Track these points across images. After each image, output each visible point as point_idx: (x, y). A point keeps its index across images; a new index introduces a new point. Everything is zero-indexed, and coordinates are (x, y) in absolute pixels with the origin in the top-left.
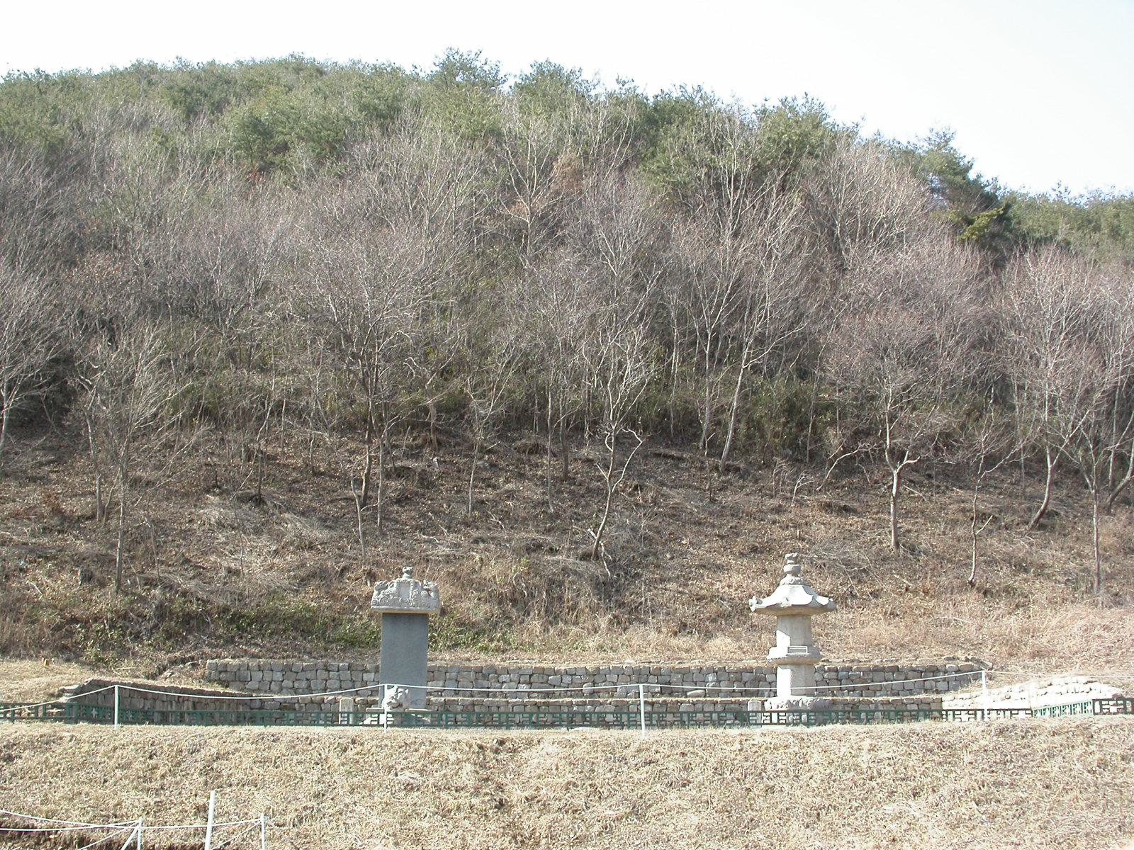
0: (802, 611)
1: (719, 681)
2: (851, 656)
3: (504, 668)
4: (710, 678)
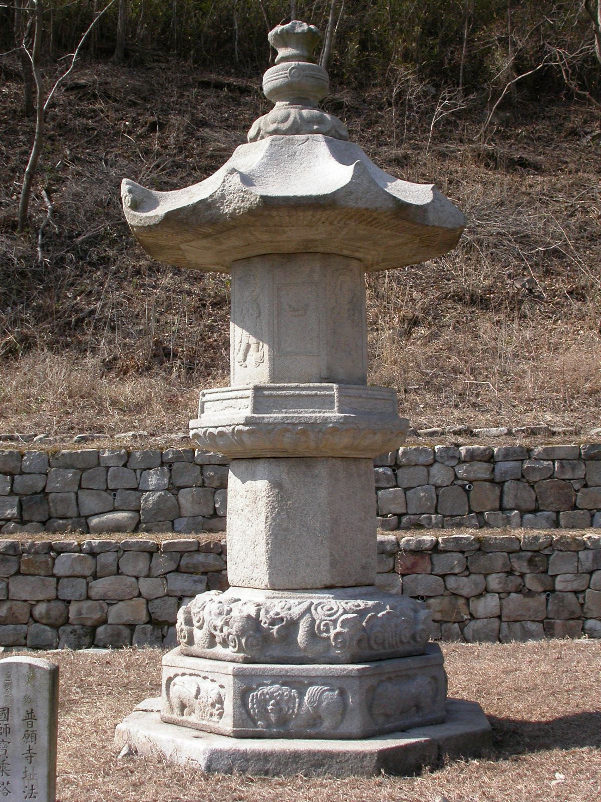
0: (319, 232)
1: (174, 489)
2: (528, 420)
4: (153, 479)
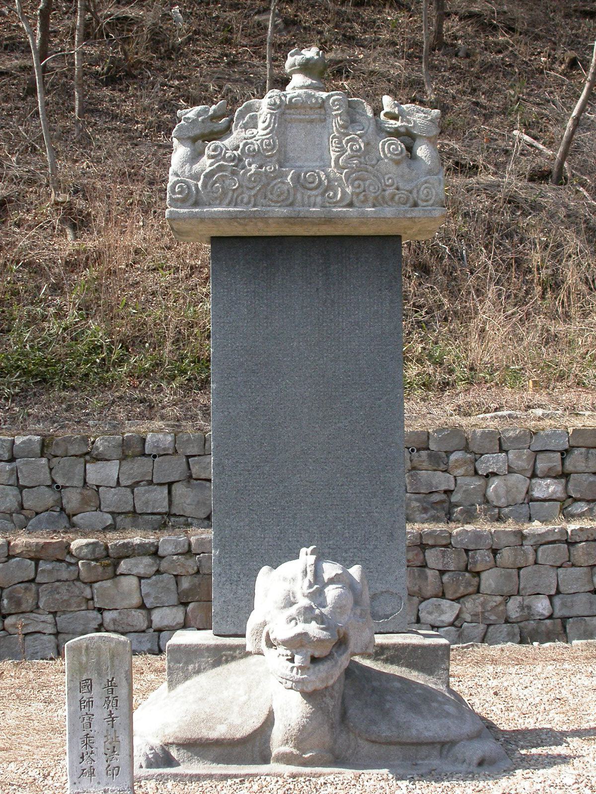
3: (488, 435)
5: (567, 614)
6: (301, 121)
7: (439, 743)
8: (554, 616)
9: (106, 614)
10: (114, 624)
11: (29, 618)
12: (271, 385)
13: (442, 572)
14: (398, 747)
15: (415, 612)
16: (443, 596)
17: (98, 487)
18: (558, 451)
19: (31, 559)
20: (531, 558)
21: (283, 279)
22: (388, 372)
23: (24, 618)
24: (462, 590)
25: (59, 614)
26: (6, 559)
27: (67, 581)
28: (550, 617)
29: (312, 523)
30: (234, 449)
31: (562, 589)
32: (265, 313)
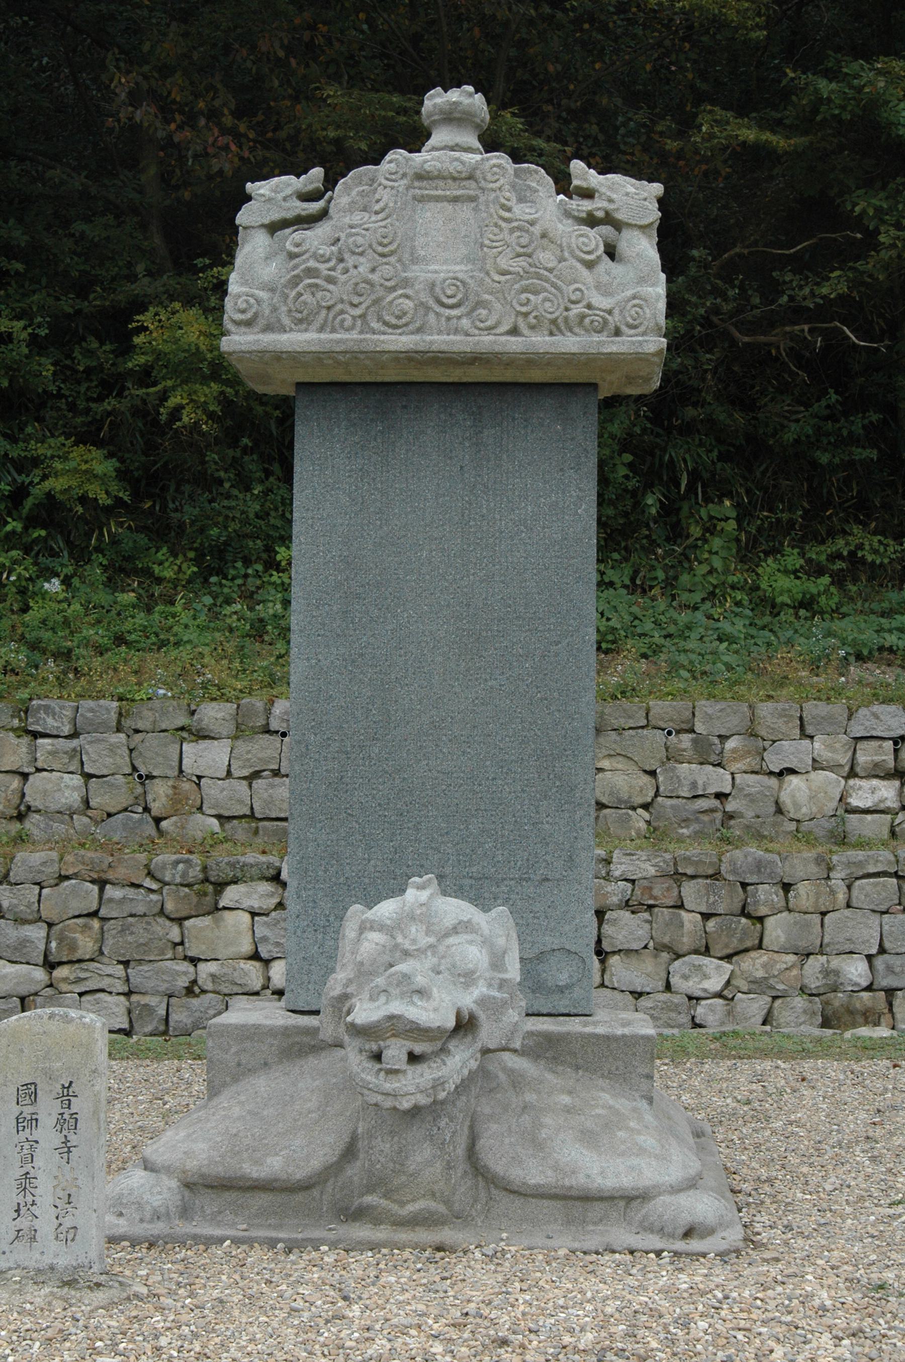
5: (895, 984)
6: (438, 199)
7: (622, 1197)
8: (875, 987)
9: (201, 966)
10: (213, 982)
11: (87, 970)
12: (385, 618)
13: (706, 916)
14: (559, 1204)
15: (664, 975)
16: (706, 951)
17: (199, 777)
18: (890, 739)
19: (93, 882)
20: (841, 897)
21: (407, 450)
22: (571, 601)
23: (82, 969)
24: (735, 944)
25: (132, 964)
26: (56, 881)
27: (145, 915)
28: (869, 988)
29: (445, 839)
30: (325, 718)
31: (887, 945)
32: (378, 504)
